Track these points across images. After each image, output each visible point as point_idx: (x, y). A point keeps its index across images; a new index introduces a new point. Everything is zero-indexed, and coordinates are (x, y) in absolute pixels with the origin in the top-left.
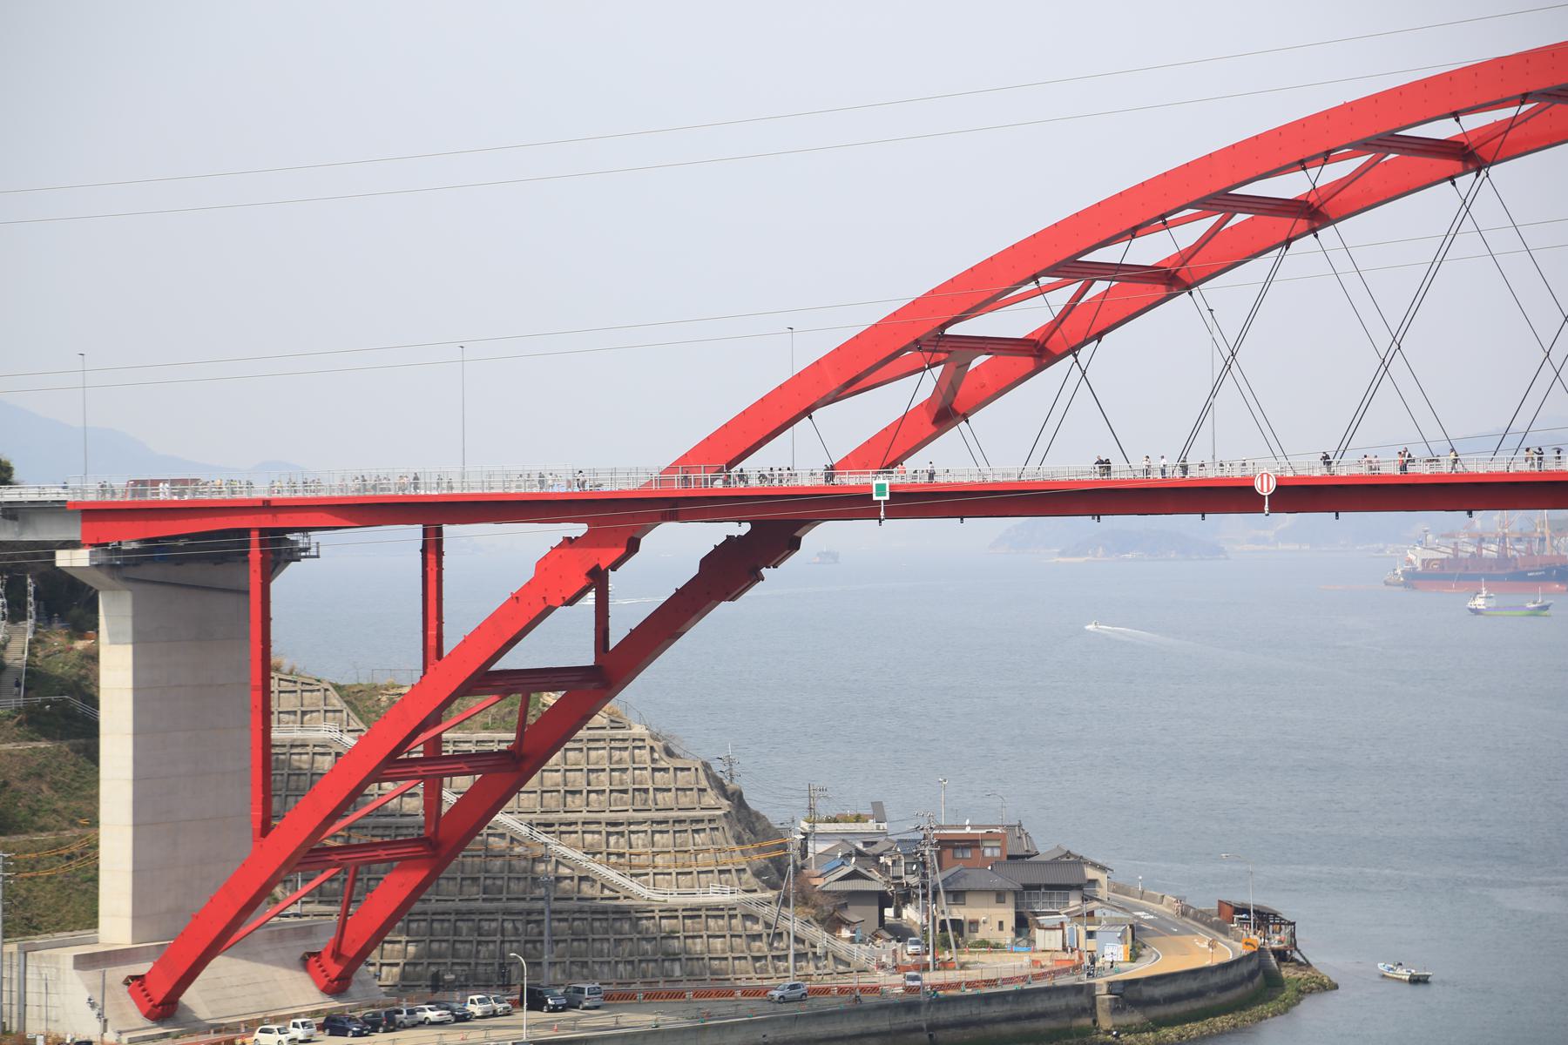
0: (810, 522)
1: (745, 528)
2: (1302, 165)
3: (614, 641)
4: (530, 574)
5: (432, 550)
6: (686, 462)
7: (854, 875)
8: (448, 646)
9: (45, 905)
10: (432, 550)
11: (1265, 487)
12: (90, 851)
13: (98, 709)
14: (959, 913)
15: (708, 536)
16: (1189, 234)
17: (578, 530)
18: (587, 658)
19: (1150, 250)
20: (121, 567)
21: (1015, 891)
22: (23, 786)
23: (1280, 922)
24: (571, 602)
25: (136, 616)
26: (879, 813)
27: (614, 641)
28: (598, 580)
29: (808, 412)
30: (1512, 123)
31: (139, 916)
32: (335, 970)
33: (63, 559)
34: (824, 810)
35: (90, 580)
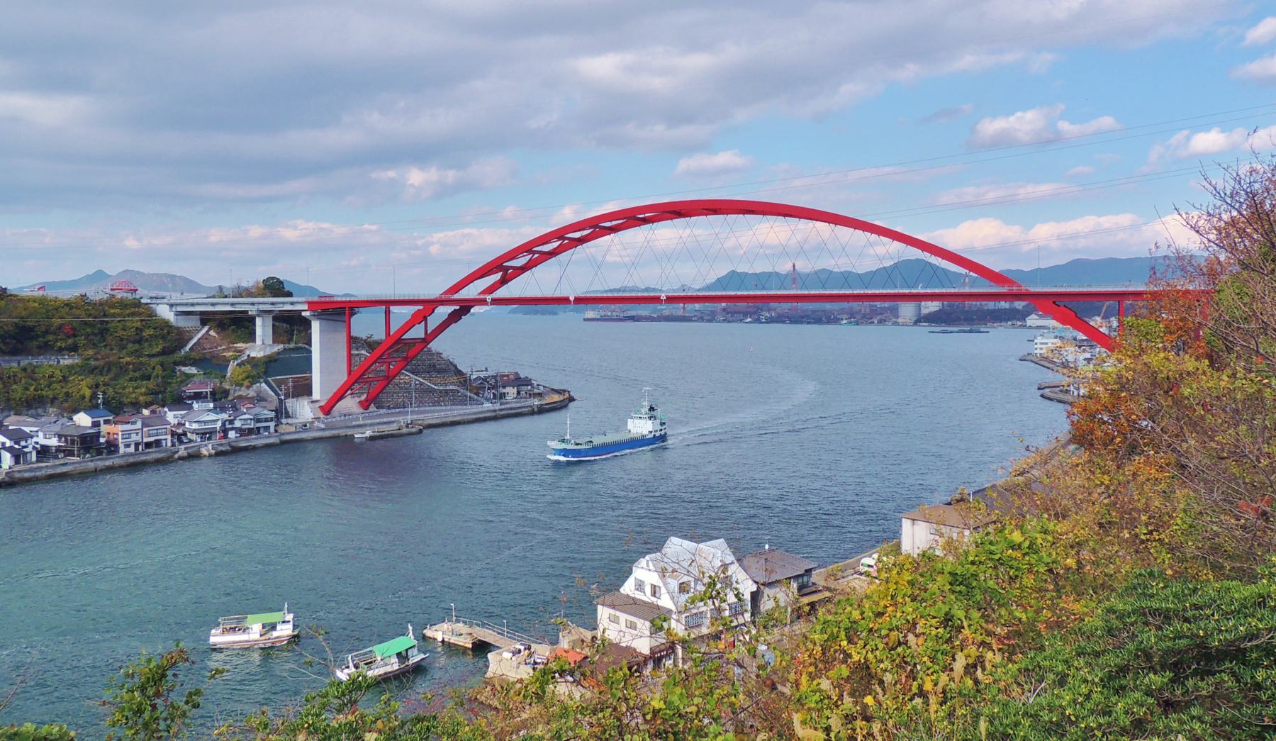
0: (472, 306)
1: (458, 307)
2: (579, 230)
3: (429, 332)
4: (409, 318)
5: (388, 313)
6: (446, 292)
7: (482, 383)
8: (391, 333)
9: (389, 729)
10: (388, 313)
11: (572, 299)
12: (310, 379)
13: (310, 346)
14: (504, 391)
15: (449, 309)
16: (556, 244)
17: (421, 307)
18: (423, 336)
19: (577, 235)
20: (318, 317)
21: (189, 378)
22: (332, 700)
23: (565, 391)
24: (419, 323)
25: (320, 326)
26: (486, 370)
27: (429, 332)
28: (425, 319)
29: (472, 282)
30: (622, 223)
31: (321, 393)
32: (1239, 706)
33: (303, 314)
34: (474, 369)
35: (310, 318)
